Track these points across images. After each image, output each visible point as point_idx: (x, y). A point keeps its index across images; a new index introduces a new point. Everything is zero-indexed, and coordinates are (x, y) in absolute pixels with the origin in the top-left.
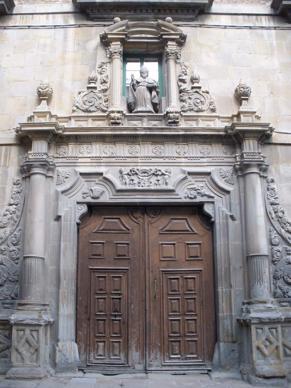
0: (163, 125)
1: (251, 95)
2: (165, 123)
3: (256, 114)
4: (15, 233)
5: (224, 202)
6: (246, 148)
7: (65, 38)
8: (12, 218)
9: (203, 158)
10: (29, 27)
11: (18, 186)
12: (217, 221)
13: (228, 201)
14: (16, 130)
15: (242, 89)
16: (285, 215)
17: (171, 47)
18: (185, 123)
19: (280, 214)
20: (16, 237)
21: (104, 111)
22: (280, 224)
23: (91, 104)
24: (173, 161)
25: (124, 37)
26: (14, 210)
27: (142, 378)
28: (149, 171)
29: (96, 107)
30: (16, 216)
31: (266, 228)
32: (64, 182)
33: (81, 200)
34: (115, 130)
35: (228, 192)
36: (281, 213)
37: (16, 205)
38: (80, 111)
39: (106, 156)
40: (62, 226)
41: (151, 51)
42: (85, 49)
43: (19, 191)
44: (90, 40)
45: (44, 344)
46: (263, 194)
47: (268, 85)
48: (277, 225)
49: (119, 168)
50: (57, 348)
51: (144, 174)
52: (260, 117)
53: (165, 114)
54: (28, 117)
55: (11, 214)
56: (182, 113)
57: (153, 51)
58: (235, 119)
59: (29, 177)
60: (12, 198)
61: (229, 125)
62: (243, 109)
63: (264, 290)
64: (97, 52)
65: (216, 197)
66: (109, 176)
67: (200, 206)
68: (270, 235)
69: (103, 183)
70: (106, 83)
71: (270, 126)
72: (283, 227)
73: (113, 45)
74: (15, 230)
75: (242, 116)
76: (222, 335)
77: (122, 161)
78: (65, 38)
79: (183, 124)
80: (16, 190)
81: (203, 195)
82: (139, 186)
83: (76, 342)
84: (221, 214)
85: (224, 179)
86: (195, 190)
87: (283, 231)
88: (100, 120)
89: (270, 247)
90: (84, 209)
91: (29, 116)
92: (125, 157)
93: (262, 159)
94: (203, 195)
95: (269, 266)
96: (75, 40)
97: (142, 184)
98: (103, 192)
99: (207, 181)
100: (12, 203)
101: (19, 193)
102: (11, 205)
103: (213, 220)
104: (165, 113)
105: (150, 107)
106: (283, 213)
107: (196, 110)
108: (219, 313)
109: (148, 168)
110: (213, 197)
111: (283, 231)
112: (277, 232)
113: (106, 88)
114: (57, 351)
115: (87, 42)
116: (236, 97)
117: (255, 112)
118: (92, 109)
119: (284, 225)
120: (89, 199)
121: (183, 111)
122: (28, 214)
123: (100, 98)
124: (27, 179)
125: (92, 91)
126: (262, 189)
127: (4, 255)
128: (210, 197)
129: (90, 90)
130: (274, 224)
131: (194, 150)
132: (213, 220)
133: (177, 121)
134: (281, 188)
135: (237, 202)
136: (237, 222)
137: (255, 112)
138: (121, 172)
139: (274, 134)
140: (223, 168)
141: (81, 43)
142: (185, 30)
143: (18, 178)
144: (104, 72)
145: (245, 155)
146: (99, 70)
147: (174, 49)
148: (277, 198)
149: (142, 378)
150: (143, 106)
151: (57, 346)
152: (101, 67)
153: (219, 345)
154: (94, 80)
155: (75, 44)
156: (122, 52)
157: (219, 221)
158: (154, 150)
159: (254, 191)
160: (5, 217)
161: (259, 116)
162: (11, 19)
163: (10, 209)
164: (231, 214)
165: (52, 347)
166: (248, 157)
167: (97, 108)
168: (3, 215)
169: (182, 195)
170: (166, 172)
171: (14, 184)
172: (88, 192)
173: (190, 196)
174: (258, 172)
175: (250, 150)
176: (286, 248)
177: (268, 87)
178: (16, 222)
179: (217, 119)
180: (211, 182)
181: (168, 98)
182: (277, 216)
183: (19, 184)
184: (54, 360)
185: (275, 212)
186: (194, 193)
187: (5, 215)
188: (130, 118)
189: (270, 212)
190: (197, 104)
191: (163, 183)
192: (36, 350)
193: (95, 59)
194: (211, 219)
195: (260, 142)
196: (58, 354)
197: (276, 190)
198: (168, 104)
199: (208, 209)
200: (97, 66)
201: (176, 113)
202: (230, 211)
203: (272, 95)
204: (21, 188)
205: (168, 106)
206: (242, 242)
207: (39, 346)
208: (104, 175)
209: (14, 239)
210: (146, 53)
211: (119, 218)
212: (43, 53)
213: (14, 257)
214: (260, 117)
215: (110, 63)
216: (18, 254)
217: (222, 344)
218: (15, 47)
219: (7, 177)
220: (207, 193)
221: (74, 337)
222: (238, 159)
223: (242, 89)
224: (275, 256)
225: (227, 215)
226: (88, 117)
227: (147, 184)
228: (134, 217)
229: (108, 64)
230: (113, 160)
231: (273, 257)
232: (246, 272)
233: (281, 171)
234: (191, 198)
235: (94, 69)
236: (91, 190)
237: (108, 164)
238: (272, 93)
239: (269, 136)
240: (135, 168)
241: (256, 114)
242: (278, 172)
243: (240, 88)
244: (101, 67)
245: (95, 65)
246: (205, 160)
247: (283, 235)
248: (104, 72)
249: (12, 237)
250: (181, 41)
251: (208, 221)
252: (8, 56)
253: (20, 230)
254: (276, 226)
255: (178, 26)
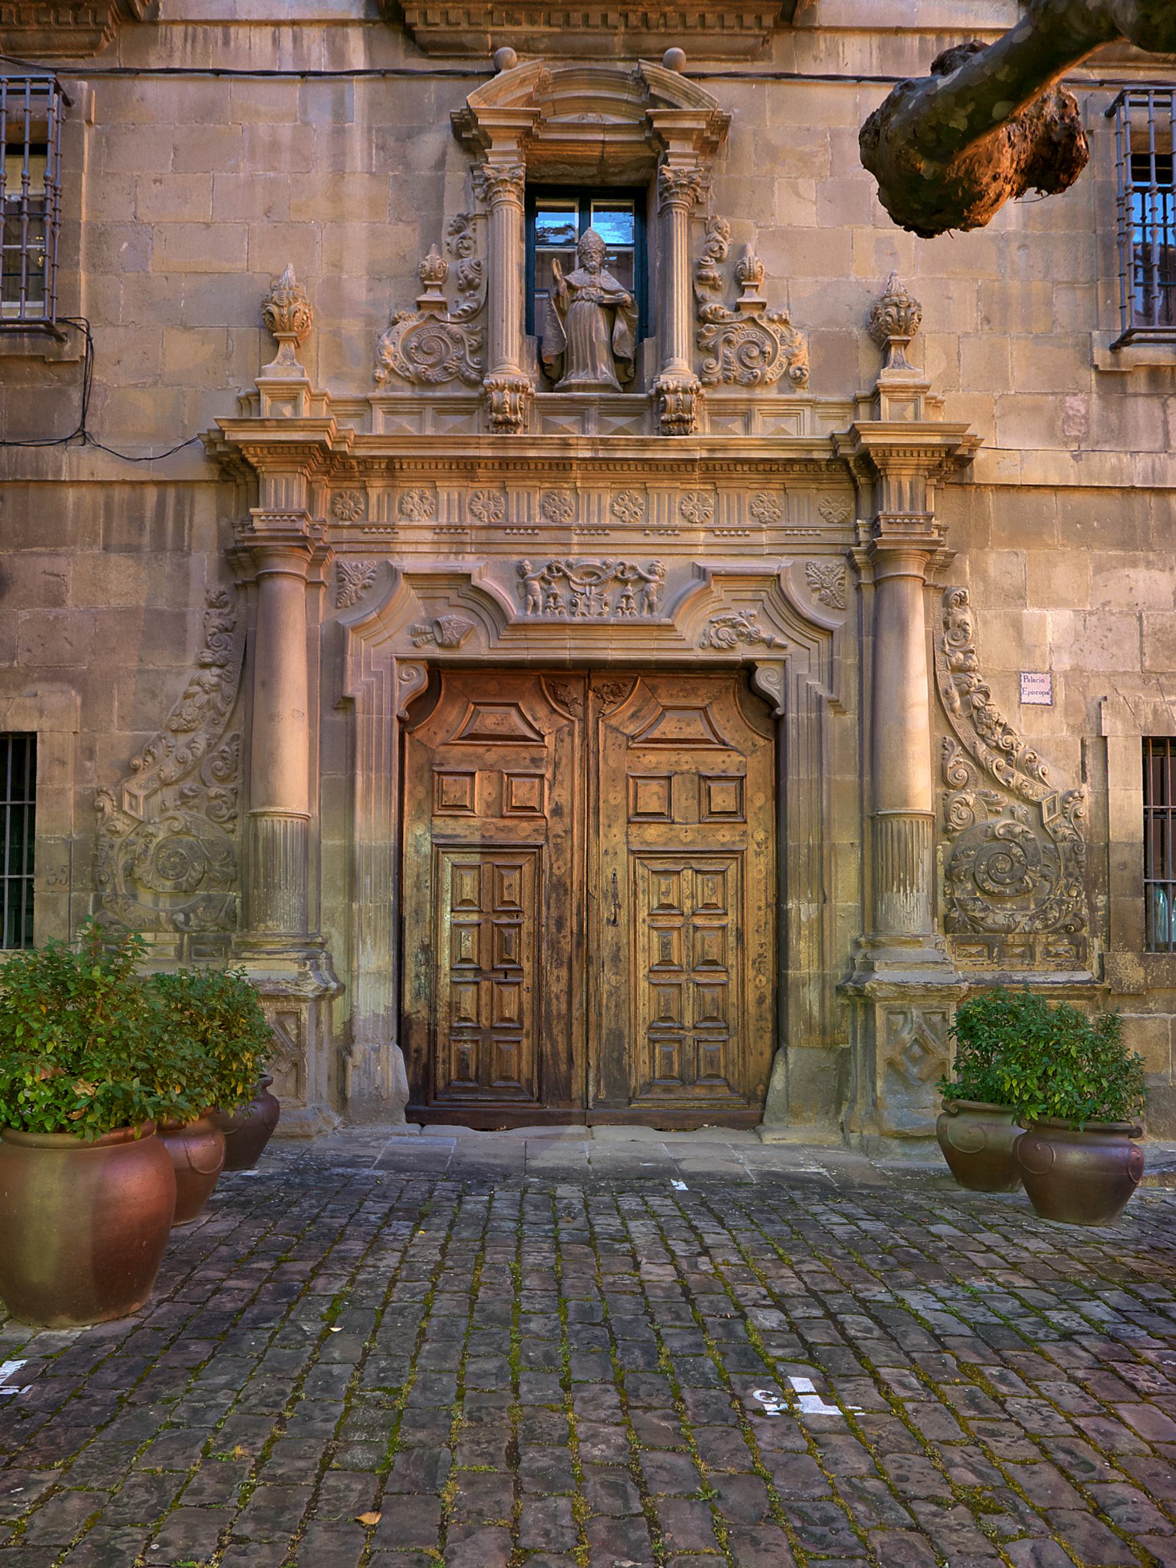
0: (646, 428)
1: (922, 327)
2: (652, 423)
3: (929, 394)
4: (223, 747)
5: (814, 661)
6: (889, 500)
7: (340, 113)
8: (210, 704)
9: (761, 530)
10: (217, 72)
11: (226, 610)
12: (791, 715)
13: (825, 660)
14: (206, 439)
15: (893, 310)
16: (992, 701)
17: (680, 161)
18: (712, 422)
19: (977, 700)
20: (224, 759)
21: (474, 384)
22: (976, 727)
23: (431, 360)
24: (672, 540)
25: (529, 123)
26: (214, 680)
27: (580, 1136)
28: (600, 569)
29: (446, 368)
30: (223, 697)
31: (932, 737)
32: (359, 598)
33: (407, 651)
34: (503, 443)
35: (830, 633)
36: (981, 696)
37: (221, 667)
38: (399, 383)
39: (479, 523)
40: (359, 729)
41: (615, 174)
42: (408, 166)
43: (229, 625)
44: (421, 131)
45: (313, 1049)
46: (931, 637)
47: (978, 292)
48: (966, 732)
49: (515, 558)
50: (350, 1060)
51: (588, 580)
52: (942, 402)
53: (650, 397)
54: (239, 399)
55: (206, 692)
56: (702, 391)
57: (620, 173)
58: (863, 409)
59: (257, 583)
60: (208, 647)
61: (839, 428)
62: (889, 377)
63: (912, 910)
64: (443, 177)
65: (792, 646)
66: (489, 583)
67: (748, 668)
68: (943, 757)
69: (470, 604)
70: (476, 288)
71: (970, 431)
72: (982, 737)
73: (494, 153)
74: (221, 737)
75: (884, 401)
76: (794, 1027)
77: (525, 539)
78: (340, 113)
79: (703, 430)
80: (217, 622)
81: (751, 640)
82: (573, 614)
83: (399, 1043)
84: (803, 694)
85: (816, 595)
86: (733, 626)
87: (982, 748)
88: (457, 412)
89: (941, 790)
90: (418, 680)
91: (242, 394)
92: (533, 529)
93: (935, 536)
94: (751, 640)
95: (935, 845)
96: (370, 129)
97: (581, 608)
98: (472, 628)
99: (767, 602)
100: (208, 660)
101: (227, 630)
102: (205, 666)
103: (779, 711)
104: (652, 392)
105: (605, 371)
106: (987, 695)
107: (745, 380)
108: (787, 968)
109: (597, 562)
110: (783, 647)
111: (982, 748)
112: (964, 748)
113: (474, 305)
114: (350, 1068)
115: (409, 137)
116: (871, 334)
117: (928, 387)
118: (433, 374)
119: (986, 731)
120: (433, 652)
121: (704, 384)
122: (259, 694)
123: (458, 341)
124: (251, 591)
125: (432, 317)
126: (926, 622)
127: (191, 808)
128: (769, 644)
129: (427, 313)
130: (955, 726)
131: (742, 504)
132: (779, 711)
133: (687, 416)
134: (985, 623)
135: (852, 661)
136: (850, 718)
137: (928, 387)
138: (521, 571)
139: (980, 455)
140: (817, 561)
141: (391, 142)
142: (722, 95)
143: (222, 588)
144: (467, 249)
145: (882, 523)
146: (454, 240)
147: (686, 169)
148: (972, 652)
149: (580, 1136)
150: (585, 366)
151: (350, 1053)
152: (458, 231)
153: (786, 1055)
154: (437, 279)
155: (370, 147)
156: (522, 182)
157: (796, 716)
158: (617, 507)
159: (902, 628)
160: (188, 701)
161: (940, 397)
162: (153, 41)
163: (204, 680)
164: (834, 696)
165: (334, 1059)
166: (895, 528)
167: (451, 374)
168: (181, 695)
169: (693, 637)
170: (650, 572)
171: (211, 605)
172: (429, 629)
173: (715, 641)
174: (921, 574)
175: (900, 507)
176: (986, 795)
177: (979, 300)
178: (223, 715)
179: (807, 411)
180: (780, 604)
181: (663, 340)
182: (967, 704)
183: (226, 604)
184: (342, 1092)
185: (964, 693)
186: (726, 632)
187: (187, 696)
188: (547, 409)
189: (947, 692)
190: (747, 361)
191: (642, 605)
192: (295, 1065)
193: (440, 206)
194: (773, 709)
195: (934, 481)
196: (352, 1077)
197: (970, 629)
198: (663, 360)
199: (767, 681)
200: (446, 229)
201: (685, 391)
202: (831, 688)
203: (986, 327)
204: (233, 617)
205: (663, 368)
206: (861, 776)
207: (303, 1055)
208: (475, 581)
209: (220, 763)
210: (598, 181)
211: (516, 705)
212: (272, 174)
213: (221, 813)
214: (942, 402)
215: (485, 216)
216: (234, 805)
217: (792, 1053)
218: (175, 149)
219: (188, 584)
220: (764, 635)
221: (393, 1033)
222: (863, 536)
223: (893, 310)
224: (954, 817)
225: (820, 699)
226: (422, 400)
227: (595, 609)
228: (557, 701)
229: (480, 223)
230: (499, 535)
231: (947, 819)
232: (868, 861)
233: (992, 571)
234: (719, 649)
235: (437, 239)
236: (438, 623)
237: (484, 548)
238: (988, 320)
239: (964, 462)
240: (562, 559)
241: (929, 394)
242: (980, 572)
243: (886, 306)
244: (458, 231)
245: (439, 223)
246: (764, 538)
247: (982, 758)
248: (467, 249)
249: (214, 759)
250: (714, 138)
251: (768, 716)
252: (155, 181)
253: (236, 737)
254: (960, 732)
255: (703, 77)
